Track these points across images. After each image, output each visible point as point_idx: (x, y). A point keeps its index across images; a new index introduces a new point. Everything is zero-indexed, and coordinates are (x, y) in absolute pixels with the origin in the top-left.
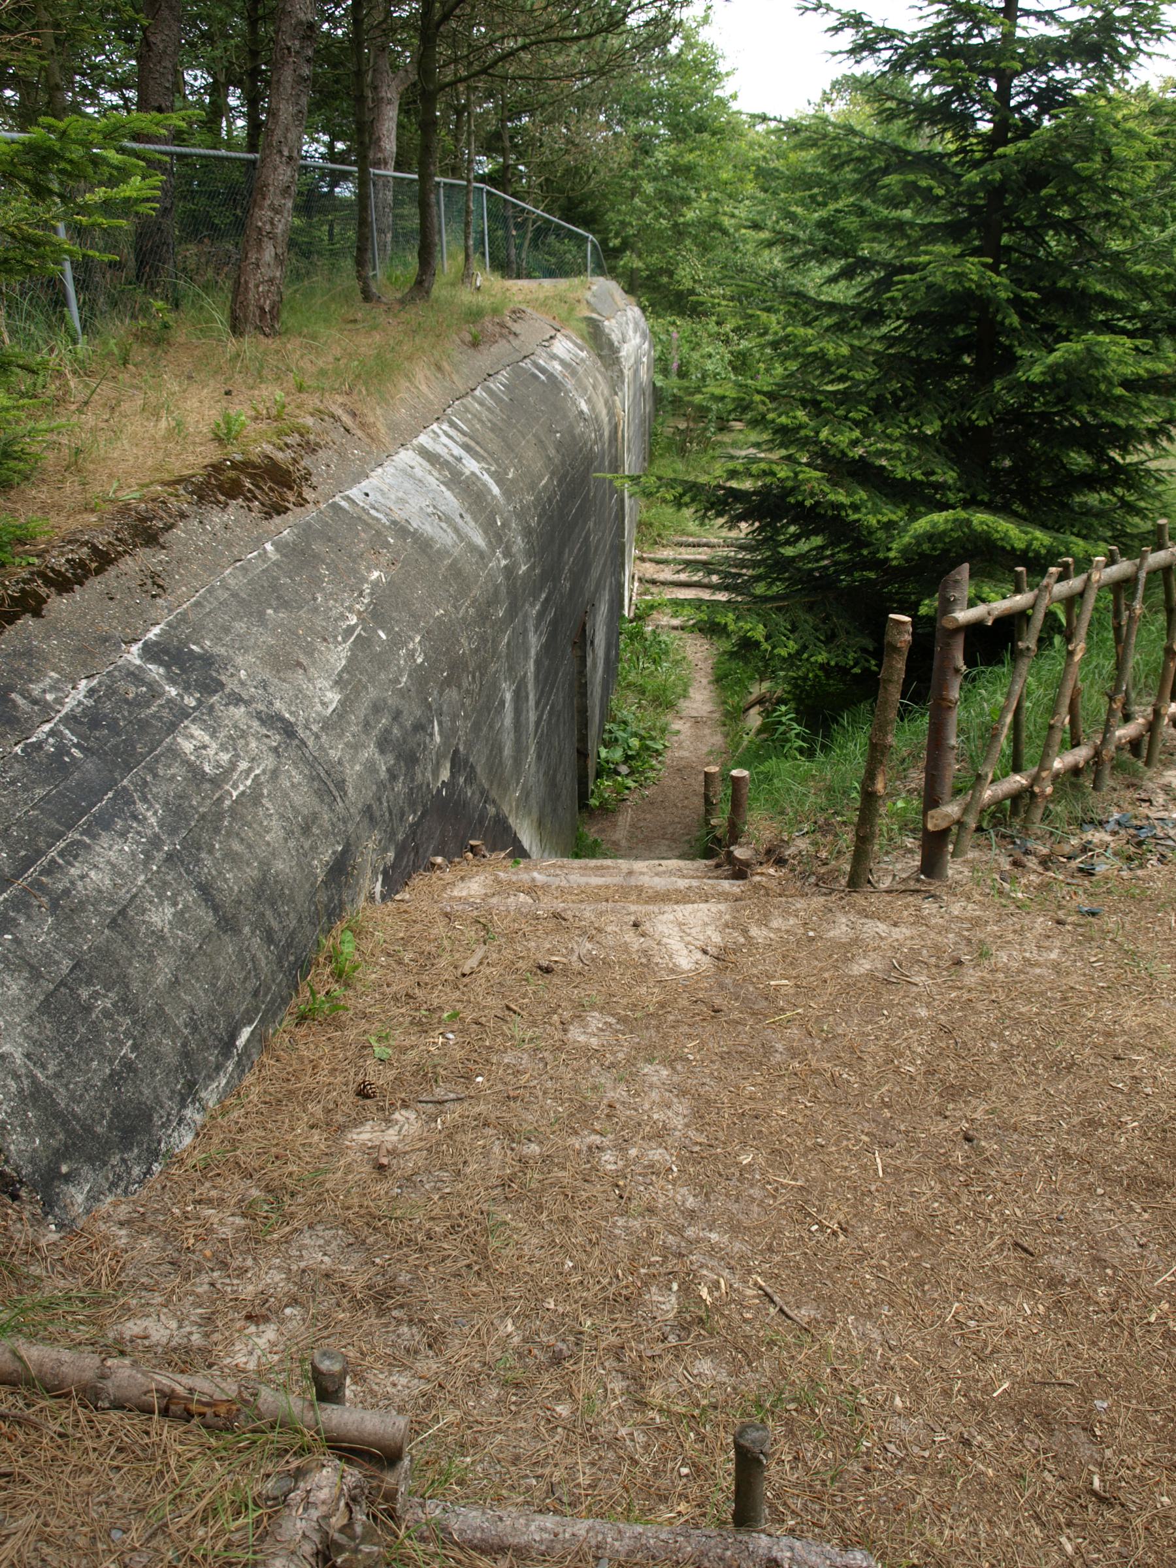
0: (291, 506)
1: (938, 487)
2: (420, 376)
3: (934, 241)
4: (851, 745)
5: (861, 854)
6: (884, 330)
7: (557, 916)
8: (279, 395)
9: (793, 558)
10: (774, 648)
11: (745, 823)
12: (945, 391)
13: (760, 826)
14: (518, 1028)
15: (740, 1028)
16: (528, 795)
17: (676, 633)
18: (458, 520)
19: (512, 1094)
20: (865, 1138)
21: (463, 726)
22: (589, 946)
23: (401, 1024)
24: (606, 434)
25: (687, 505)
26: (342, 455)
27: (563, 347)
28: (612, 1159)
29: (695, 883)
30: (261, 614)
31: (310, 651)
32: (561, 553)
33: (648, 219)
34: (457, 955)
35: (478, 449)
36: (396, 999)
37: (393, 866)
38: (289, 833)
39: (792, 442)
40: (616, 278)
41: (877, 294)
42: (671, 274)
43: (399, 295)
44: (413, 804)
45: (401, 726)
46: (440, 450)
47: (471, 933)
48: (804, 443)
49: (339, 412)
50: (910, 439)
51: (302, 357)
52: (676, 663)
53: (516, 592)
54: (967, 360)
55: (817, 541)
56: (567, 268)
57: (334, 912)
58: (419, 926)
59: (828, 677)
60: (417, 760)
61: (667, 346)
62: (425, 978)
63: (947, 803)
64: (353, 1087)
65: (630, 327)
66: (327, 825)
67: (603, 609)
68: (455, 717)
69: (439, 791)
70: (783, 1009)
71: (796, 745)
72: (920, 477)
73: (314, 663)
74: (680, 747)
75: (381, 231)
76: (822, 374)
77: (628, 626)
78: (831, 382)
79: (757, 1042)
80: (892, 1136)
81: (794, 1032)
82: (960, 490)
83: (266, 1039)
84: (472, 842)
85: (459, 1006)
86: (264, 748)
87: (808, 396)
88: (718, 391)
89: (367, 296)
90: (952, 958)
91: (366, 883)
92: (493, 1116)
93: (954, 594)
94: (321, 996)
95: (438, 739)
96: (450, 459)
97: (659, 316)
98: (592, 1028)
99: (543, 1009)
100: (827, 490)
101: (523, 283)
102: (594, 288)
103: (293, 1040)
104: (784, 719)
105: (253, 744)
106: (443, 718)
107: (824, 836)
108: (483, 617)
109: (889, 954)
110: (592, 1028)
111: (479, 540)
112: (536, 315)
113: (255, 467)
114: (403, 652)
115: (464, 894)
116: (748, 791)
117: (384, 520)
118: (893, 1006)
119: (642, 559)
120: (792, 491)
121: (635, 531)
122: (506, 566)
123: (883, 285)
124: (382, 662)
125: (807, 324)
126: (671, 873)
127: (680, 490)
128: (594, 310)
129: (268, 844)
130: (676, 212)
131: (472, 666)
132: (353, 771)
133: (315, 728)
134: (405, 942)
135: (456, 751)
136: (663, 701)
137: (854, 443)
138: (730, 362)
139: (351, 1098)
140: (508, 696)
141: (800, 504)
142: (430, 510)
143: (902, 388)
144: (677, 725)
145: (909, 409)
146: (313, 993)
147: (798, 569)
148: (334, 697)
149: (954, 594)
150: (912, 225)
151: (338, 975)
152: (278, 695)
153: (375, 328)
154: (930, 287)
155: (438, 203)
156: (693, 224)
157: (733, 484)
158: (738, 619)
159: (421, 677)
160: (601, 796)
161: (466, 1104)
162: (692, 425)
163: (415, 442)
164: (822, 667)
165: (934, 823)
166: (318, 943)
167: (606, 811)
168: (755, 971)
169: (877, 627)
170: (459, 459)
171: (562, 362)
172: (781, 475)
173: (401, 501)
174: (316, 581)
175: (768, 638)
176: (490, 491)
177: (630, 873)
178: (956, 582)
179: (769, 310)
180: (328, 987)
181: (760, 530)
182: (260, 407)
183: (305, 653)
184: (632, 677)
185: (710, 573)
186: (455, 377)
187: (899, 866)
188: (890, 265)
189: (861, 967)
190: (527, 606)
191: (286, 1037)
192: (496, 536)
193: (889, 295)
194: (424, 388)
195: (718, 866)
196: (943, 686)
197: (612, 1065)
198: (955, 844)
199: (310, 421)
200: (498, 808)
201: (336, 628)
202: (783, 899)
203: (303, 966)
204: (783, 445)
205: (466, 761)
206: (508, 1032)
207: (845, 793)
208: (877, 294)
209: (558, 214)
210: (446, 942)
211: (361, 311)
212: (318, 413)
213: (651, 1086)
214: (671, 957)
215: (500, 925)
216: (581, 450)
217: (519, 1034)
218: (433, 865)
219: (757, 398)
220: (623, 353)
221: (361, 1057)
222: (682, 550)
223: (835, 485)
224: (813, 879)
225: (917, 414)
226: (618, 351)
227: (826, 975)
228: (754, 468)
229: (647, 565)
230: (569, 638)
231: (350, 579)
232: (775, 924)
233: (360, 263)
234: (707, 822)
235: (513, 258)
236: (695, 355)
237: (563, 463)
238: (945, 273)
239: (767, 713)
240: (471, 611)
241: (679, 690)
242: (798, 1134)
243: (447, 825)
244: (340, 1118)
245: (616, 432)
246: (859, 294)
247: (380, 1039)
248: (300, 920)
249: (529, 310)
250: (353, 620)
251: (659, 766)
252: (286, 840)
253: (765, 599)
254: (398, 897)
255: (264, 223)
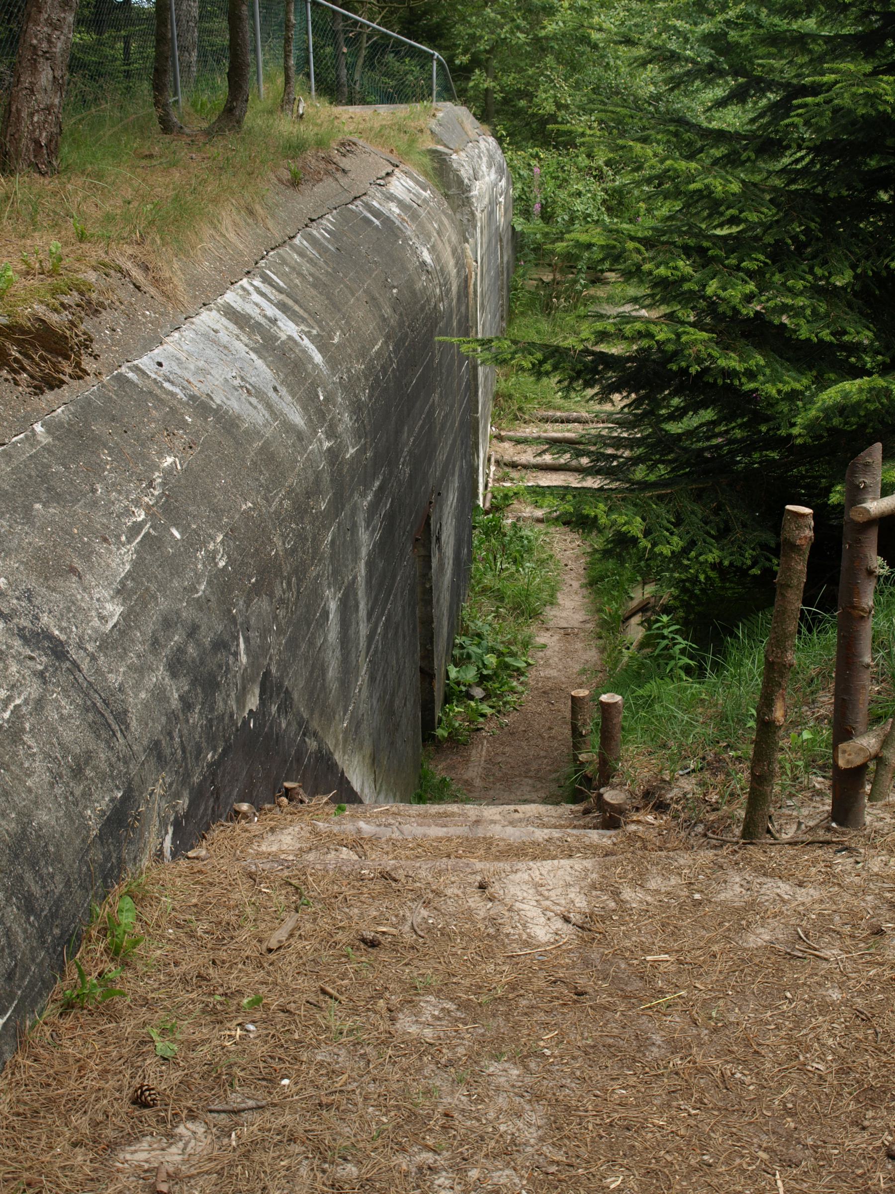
0: (66, 378)
1: (855, 349)
2: (227, 222)
3: (842, 57)
4: (748, 662)
5: (757, 798)
6: (786, 161)
7: (386, 876)
8: (55, 245)
9: (679, 435)
10: (654, 545)
11: (618, 759)
12: (857, 234)
13: (637, 763)
14: (334, 1017)
15: (609, 1015)
16: (358, 726)
17: (541, 527)
18: (271, 394)
19: (325, 1100)
20: (762, 1155)
21: (276, 643)
22: (424, 913)
23: (190, 1012)
24: (454, 289)
25: (547, 374)
26: (130, 317)
27: (401, 185)
28: (447, 1183)
29: (556, 834)
30: (28, 510)
31: (87, 554)
32: (398, 432)
33: (503, 33)
34: (262, 926)
35: (297, 308)
36: (184, 981)
37: (187, 816)
38: (57, 777)
39: (675, 298)
40: (465, 103)
41: (775, 120)
42: (530, 96)
43: (205, 125)
44: (212, 740)
45: (198, 644)
46: (254, 312)
47: (280, 898)
48: (688, 299)
49: (128, 265)
50: (817, 291)
51: (85, 199)
52: (542, 563)
53: (342, 479)
54: (884, 196)
55: (708, 415)
56: (409, 91)
57: (111, 873)
58: (216, 890)
59: (723, 579)
60: (218, 685)
61: (528, 183)
62: (224, 955)
63: (862, 734)
64: (128, 1093)
65: (484, 163)
66: (104, 766)
67: (452, 499)
68: (265, 632)
69: (246, 723)
70: (661, 991)
71: (681, 663)
72: (828, 338)
73: (91, 568)
74: (547, 665)
75: (183, 49)
76: (710, 216)
77: (483, 518)
78: (721, 225)
79: (629, 1033)
80: (797, 1152)
81: (676, 1020)
82: (878, 353)
83: (22, 1033)
84: (287, 785)
85: (263, 989)
86: (27, 673)
87: (692, 242)
88: (584, 238)
89: (167, 126)
90: (871, 926)
91: (152, 840)
92: (300, 1129)
93: (864, 480)
94: (92, 979)
95: (244, 659)
96: (263, 321)
97: (519, 148)
98: (426, 1017)
99: (367, 993)
100: (715, 354)
101: (355, 110)
102: (440, 115)
103: (56, 1034)
104: (666, 632)
105: (14, 669)
106: (251, 634)
107: (714, 775)
108: (301, 511)
109: (793, 921)
110: (426, 1017)
111: (297, 418)
112: (369, 148)
113: (23, 331)
114: (201, 554)
115: (274, 848)
116: (621, 719)
117: (181, 395)
118: (798, 987)
119: (500, 439)
120: (675, 355)
121: (491, 404)
122: (329, 449)
123: (782, 109)
124: (175, 566)
125: (690, 157)
126: (528, 821)
127: (539, 355)
128: (439, 142)
129: (30, 790)
130: (536, 24)
131: (286, 569)
132: (136, 700)
133: (91, 647)
134: (199, 910)
135: (267, 674)
136: (526, 609)
137: (749, 298)
138: (604, 201)
139: (125, 1107)
140: (333, 606)
141: (684, 371)
142: (237, 382)
143: (807, 231)
144: (542, 639)
145: (814, 256)
146: (82, 975)
147: (685, 449)
148: (115, 610)
149: (864, 480)
150: (814, 37)
151: (115, 952)
152: (45, 608)
153: (174, 164)
154: (836, 110)
155: (253, 16)
156: (554, 37)
157: (603, 348)
158: (611, 510)
159: (223, 585)
160: (450, 725)
161: (267, 1114)
162: (558, 276)
163: (220, 301)
164: (713, 566)
165: (849, 756)
166: (90, 913)
167: (456, 743)
168: (628, 943)
169: (775, 518)
170: (274, 321)
171: (401, 203)
172: (661, 337)
173: (201, 371)
174: (96, 469)
175: (647, 533)
176: (310, 359)
177: (477, 822)
178: (867, 465)
179: (645, 140)
180: (101, 967)
181: (637, 403)
182: (32, 260)
183: (81, 556)
184: (488, 580)
185: (579, 454)
186: (270, 224)
187: (805, 812)
188: (789, 84)
189: (759, 937)
190: (356, 496)
191: (48, 1030)
192: (318, 413)
193: (787, 121)
194: (231, 236)
195: (586, 812)
196: (854, 591)
197: (450, 1063)
198: (874, 784)
199: (92, 277)
200: (320, 741)
201: (119, 525)
202: (663, 853)
203: (72, 941)
204: (664, 301)
205: (280, 686)
206: (322, 1022)
207: (741, 722)
208: (775, 120)
209: (397, 28)
210: (249, 910)
211: (158, 144)
212: (102, 267)
213: (498, 1089)
214: (524, 926)
215: (316, 889)
216: (422, 309)
217: (335, 1024)
218: (237, 813)
219: (630, 245)
220: (475, 193)
221: (139, 1055)
222: (548, 426)
223: (726, 348)
224: (700, 829)
225: (824, 263)
226: (468, 189)
227: (715, 948)
228: (628, 329)
229: (506, 445)
230: (409, 533)
231: (137, 466)
232: (652, 885)
233: (158, 87)
234: (575, 758)
235: (344, 80)
236: (563, 194)
237: (401, 324)
238: (854, 95)
239: (648, 624)
240: (287, 503)
241: (545, 595)
242: (679, 1150)
243: (258, 763)
244: (110, 1133)
245: (466, 287)
246: (752, 121)
247: (163, 1032)
248: (68, 884)
249: (361, 142)
250: (141, 516)
251: (520, 688)
252: (52, 785)
253: (644, 485)
254: (191, 854)
255: (40, 41)
